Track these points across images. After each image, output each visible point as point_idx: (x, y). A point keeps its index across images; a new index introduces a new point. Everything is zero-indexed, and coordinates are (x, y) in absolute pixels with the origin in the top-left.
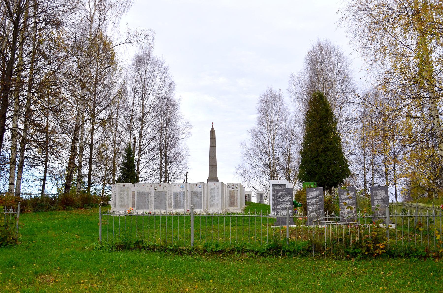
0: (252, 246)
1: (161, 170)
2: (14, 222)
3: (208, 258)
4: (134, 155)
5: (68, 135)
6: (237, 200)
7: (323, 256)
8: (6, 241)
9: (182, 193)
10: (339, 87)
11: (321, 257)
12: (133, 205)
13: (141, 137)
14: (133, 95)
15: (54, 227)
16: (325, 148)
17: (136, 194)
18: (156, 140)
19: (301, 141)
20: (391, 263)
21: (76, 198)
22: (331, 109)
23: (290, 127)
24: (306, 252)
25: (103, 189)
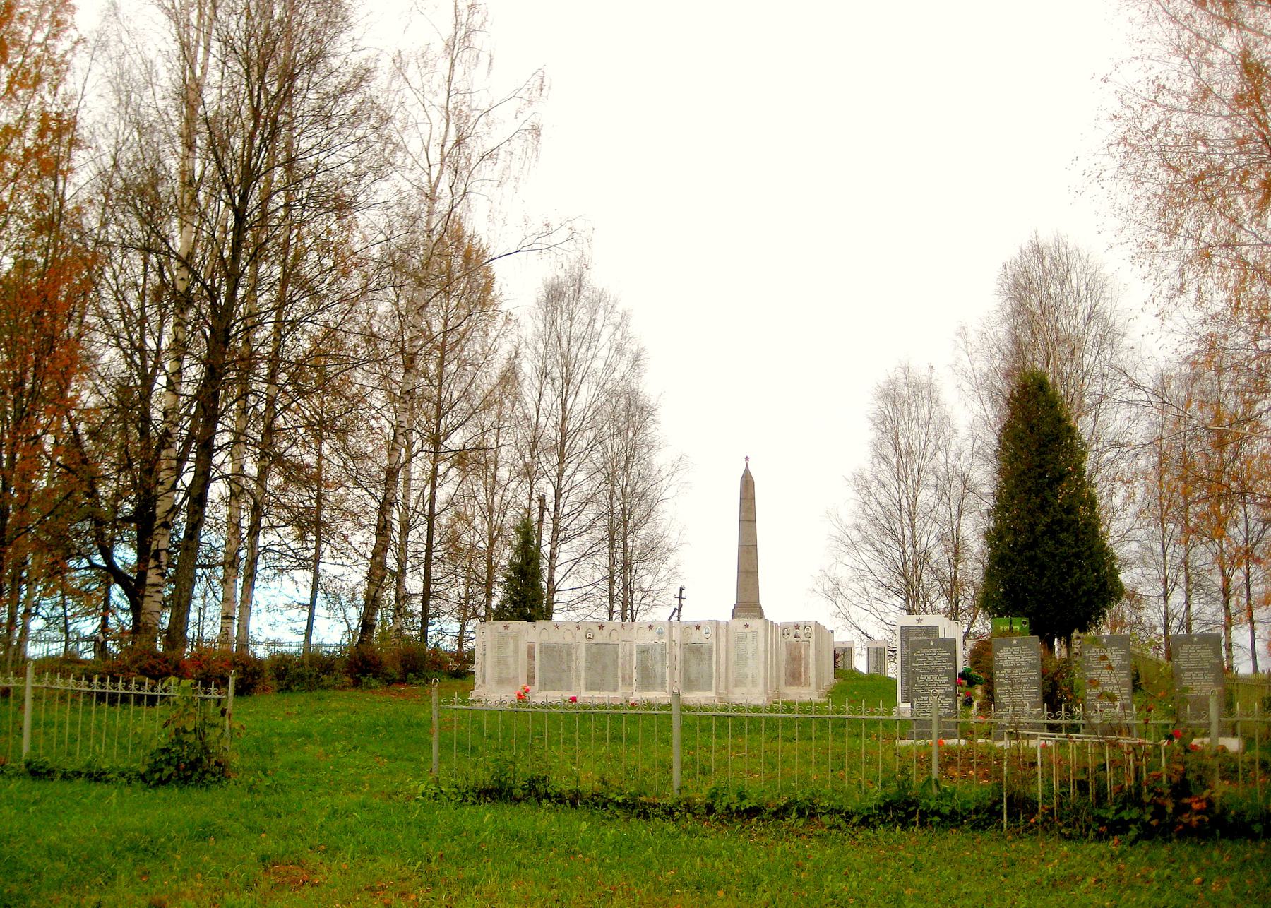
0: (837, 797)
1: (612, 582)
2: (219, 720)
3: (719, 830)
4: (539, 542)
5: (370, 493)
6: (807, 668)
7: (1031, 827)
8: (200, 770)
9: (659, 649)
10: (1089, 359)
11: (1025, 830)
12: (531, 679)
13: (558, 494)
14: (537, 384)
15: (324, 735)
16: (1053, 522)
17: (537, 650)
18: (598, 503)
19: (988, 503)
20: (1222, 854)
21: (385, 659)
22: (1068, 417)
23: (958, 467)
24: (983, 817)
25: (462, 631)
